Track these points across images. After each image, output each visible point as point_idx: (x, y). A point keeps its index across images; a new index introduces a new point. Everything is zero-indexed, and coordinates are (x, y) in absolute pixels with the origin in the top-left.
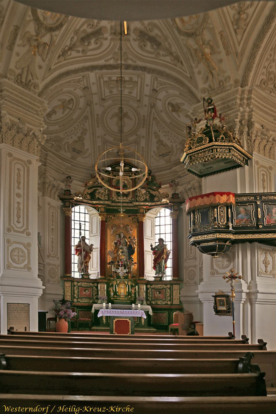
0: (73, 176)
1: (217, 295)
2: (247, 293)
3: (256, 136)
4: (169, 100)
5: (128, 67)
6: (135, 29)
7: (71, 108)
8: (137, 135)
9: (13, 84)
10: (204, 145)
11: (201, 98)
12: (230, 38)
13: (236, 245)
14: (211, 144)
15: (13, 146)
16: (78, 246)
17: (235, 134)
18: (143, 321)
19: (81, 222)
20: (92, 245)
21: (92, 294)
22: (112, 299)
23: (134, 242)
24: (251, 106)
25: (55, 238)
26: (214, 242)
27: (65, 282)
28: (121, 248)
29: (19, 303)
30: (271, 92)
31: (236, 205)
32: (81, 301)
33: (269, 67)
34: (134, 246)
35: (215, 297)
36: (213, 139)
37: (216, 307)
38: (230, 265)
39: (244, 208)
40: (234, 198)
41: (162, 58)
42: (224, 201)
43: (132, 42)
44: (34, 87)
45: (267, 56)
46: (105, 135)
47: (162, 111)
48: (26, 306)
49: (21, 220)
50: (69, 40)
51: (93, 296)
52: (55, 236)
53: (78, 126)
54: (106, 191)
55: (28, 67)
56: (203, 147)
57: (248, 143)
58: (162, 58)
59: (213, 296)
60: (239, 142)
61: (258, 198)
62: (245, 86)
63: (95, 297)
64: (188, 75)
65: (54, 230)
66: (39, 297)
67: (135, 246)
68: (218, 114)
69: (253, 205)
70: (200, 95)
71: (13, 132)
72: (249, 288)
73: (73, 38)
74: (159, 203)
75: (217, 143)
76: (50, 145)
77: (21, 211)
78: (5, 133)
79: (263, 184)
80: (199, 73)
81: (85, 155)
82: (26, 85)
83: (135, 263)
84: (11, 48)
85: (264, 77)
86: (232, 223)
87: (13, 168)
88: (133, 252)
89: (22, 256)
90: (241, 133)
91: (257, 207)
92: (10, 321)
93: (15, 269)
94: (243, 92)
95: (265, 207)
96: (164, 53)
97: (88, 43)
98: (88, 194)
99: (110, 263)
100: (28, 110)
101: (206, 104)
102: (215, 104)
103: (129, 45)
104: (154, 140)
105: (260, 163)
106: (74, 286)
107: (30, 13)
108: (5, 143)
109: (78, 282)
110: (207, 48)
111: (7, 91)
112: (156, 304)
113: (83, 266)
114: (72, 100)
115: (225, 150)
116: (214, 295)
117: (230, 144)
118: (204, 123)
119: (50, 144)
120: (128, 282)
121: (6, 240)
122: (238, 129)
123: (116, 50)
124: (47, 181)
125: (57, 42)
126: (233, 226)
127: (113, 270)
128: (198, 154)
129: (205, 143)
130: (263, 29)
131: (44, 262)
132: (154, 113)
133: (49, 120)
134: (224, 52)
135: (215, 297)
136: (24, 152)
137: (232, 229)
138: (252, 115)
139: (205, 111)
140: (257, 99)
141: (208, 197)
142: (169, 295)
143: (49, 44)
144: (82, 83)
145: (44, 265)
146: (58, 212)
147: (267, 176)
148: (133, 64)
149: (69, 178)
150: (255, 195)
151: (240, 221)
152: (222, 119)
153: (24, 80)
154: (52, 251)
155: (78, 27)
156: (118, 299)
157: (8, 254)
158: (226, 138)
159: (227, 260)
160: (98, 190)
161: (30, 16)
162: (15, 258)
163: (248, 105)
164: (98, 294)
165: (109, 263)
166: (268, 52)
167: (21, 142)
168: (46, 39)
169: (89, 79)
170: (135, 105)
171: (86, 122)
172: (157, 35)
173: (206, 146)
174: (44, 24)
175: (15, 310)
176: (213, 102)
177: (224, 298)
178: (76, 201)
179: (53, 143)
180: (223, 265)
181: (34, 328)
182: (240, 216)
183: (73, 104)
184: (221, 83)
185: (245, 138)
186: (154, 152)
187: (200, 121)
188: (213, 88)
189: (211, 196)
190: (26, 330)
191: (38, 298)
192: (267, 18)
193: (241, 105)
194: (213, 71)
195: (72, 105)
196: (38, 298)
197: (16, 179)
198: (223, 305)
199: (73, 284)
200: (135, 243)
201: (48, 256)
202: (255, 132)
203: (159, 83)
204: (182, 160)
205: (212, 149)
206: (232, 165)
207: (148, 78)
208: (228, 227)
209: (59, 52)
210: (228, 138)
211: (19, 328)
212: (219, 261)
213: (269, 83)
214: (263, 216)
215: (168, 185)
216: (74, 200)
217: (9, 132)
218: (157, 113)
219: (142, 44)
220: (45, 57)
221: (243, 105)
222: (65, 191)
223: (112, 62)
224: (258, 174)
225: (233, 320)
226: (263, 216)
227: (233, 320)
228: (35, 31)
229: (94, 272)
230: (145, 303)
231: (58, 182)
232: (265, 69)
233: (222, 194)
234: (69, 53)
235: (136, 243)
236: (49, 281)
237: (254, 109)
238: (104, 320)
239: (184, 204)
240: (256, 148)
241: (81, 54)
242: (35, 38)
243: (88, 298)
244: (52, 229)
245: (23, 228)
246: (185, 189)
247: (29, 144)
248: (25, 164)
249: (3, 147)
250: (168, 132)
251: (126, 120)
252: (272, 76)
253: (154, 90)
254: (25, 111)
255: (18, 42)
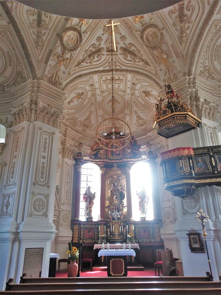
0: (83, 143)
1: (190, 233)
2: (214, 231)
3: (202, 107)
4: (143, 89)
5: (117, 70)
6: (121, 48)
7: (82, 98)
8: (124, 113)
9: (47, 83)
10: (168, 115)
11: (163, 85)
12: (178, 47)
13: (200, 188)
14: (173, 114)
15: (43, 123)
16: (85, 194)
17: (188, 107)
18: (133, 259)
19: (88, 176)
20: (95, 193)
21: (94, 235)
22: (109, 238)
23: (124, 189)
24: (196, 88)
25: (69, 189)
26: (182, 186)
27: (74, 225)
28: (115, 195)
29: (35, 248)
30: (207, 78)
31: (195, 157)
32: (86, 242)
33: (204, 63)
34: (124, 192)
35: (189, 235)
36: (174, 110)
37: (191, 244)
38: (196, 206)
39: (201, 159)
40: (193, 151)
41: (137, 63)
42: (186, 154)
43: (119, 55)
44: (59, 85)
45: (202, 56)
46: (104, 114)
47: (139, 97)
48: (39, 250)
49: (44, 175)
50: (82, 56)
51: (95, 236)
52: (69, 188)
53: (87, 109)
54: (105, 152)
55: (56, 72)
56: (167, 116)
57: (197, 112)
58: (137, 63)
59: (187, 234)
60: (191, 111)
61: (210, 150)
62: (191, 75)
63: (96, 238)
64: (154, 72)
65: (69, 183)
66: (52, 241)
67: (125, 192)
68: (175, 94)
69: (207, 155)
70: (162, 84)
71: (44, 113)
72: (215, 225)
73: (84, 55)
74: (140, 159)
75: (176, 113)
76: (69, 123)
77: (45, 169)
78: (38, 114)
79: (212, 140)
80: (161, 70)
81: (91, 129)
82: (54, 83)
83: (126, 206)
84: (46, 62)
85: (202, 69)
86: (194, 171)
87: (42, 137)
88: (123, 198)
89: (42, 205)
90: (192, 106)
91: (211, 157)
92: (26, 266)
93: (36, 217)
94: (190, 79)
95: (216, 156)
96: (138, 60)
97: (93, 57)
98: (93, 155)
99: (107, 207)
100: (55, 99)
101: (167, 89)
102: (173, 89)
103: (117, 57)
104: (135, 116)
105: (207, 125)
106: (81, 228)
107: (59, 42)
108: (38, 121)
109: (84, 225)
110: (164, 55)
111: (42, 87)
112: (143, 242)
113: (88, 211)
114: (83, 93)
115: (183, 118)
116: (188, 233)
117: (185, 113)
118: (167, 101)
119: (69, 121)
120: (121, 223)
121: (32, 193)
122: (189, 103)
123: (110, 61)
124: (66, 147)
125: (74, 57)
126: (195, 173)
127: (109, 213)
128: (164, 121)
129: (169, 114)
130: (198, 41)
131: (59, 209)
132: (134, 99)
133: (69, 106)
134: (175, 56)
135: (189, 235)
136: (46, 125)
137: (195, 175)
138: (198, 93)
139: (167, 93)
140: (199, 83)
141: (170, 153)
142: (152, 233)
143: (69, 58)
144: (90, 82)
145: (59, 211)
146: (72, 168)
147: (213, 133)
148: (120, 68)
149: (81, 144)
150: (208, 148)
151: (200, 169)
152: (178, 97)
153: (53, 81)
154: (66, 199)
155: (87, 49)
156: (113, 238)
157: (32, 204)
158: (182, 109)
159: (194, 201)
160: (99, 152)
161: (59, 43)
162: (37, 207)
163: (194, 87)
164: (98, 234)
165: (107, 207)
166: (203, 53)
167: (49, 120)
168: (68, 56)
169: (94, 79)
170: (122, 94)
171: (92, 106)
172: (134, 50)
173: (169, 116)
174: (67, 48)
175: (31, 255)
176: (171, 88)
177: (196, 236)
178: (85, 160)
179: (71, 121)
180: (191, 205)
181: (45, 274)
182: (199, 165)
183: (84, 96)
184: (175, 75)
185: (195, 109)
186: (135, 124)
187: (164, 99)
188: (170, 79)
189: (180, 150)
190: (40, 276)
191: (52, 242)
192: (199, 35)
193: (189, 87)
194: (169, 69)
195: (83, 96)
196: (52, 242)
197: (43, 146)
198: (196, 243)
199: (80, 226)
200: (125, 190)
201: (63, 204)
202: (201, 104)
203: (136, 79)
204: (153, 127)
205: (174, 118)
206: (189, 128)
207: (129, 76)
208: (192, 173)
209: (76, 63)
210: (184, 109)
211: (32, 274)
212: (188, 202)
213: (206, 72)
214: (216, 164)
215: (145, 146)
216: (83, 160)
217: (42, 113)
218: (136, 99)
219: (125, 57)
220: (67, 66)
221: (191, 87)
222: (78, 153)
223: (107, 68)
224: (207, 133)
225: (209, 259)
226: (216, 164)
227: (209, 259)
228: (62, 51)
229: (96, 216)
230: (134, 241)
231: (73, 147)
232: (202, 64)
233: (184, 149)
234: (82, 64)
235: (126, 190)
236: (62, 225)
237: (198, 89)
238: (103, 259)
239: (157, 158)
240: (203, 115)
241: (89, 64)
242: (61, 56)
243: (91, 238)
244: (68, 182)
245: (45, 182)
246: (157, 148)
247: (54, 122)
248: (51, 135)
249: (36, 123)
250: (144, 110)
251: (116, 104)
252: (207, 68)
253: (134, 84)
254: (53, 100)
255: (51, 58)
